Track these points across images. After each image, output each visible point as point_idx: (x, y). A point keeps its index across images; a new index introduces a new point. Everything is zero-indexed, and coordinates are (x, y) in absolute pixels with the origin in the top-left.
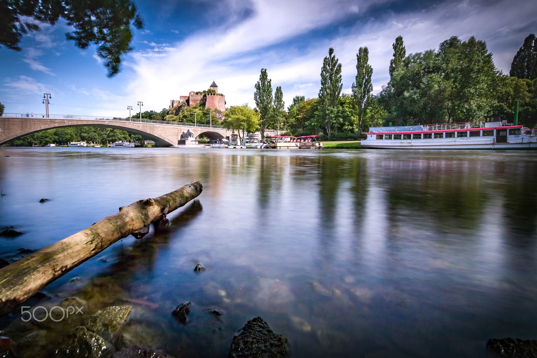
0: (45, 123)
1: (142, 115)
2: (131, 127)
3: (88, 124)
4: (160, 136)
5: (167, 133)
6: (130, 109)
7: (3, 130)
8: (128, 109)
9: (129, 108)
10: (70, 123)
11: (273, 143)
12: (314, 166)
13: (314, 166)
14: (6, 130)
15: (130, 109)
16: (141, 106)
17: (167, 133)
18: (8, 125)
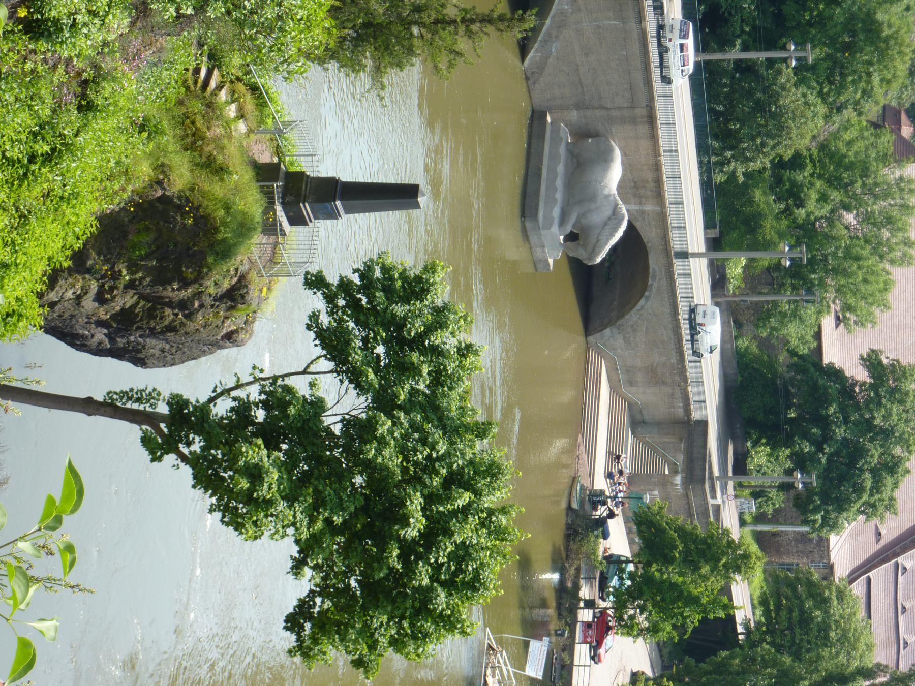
4: (561, 25)
17: (587, 55)
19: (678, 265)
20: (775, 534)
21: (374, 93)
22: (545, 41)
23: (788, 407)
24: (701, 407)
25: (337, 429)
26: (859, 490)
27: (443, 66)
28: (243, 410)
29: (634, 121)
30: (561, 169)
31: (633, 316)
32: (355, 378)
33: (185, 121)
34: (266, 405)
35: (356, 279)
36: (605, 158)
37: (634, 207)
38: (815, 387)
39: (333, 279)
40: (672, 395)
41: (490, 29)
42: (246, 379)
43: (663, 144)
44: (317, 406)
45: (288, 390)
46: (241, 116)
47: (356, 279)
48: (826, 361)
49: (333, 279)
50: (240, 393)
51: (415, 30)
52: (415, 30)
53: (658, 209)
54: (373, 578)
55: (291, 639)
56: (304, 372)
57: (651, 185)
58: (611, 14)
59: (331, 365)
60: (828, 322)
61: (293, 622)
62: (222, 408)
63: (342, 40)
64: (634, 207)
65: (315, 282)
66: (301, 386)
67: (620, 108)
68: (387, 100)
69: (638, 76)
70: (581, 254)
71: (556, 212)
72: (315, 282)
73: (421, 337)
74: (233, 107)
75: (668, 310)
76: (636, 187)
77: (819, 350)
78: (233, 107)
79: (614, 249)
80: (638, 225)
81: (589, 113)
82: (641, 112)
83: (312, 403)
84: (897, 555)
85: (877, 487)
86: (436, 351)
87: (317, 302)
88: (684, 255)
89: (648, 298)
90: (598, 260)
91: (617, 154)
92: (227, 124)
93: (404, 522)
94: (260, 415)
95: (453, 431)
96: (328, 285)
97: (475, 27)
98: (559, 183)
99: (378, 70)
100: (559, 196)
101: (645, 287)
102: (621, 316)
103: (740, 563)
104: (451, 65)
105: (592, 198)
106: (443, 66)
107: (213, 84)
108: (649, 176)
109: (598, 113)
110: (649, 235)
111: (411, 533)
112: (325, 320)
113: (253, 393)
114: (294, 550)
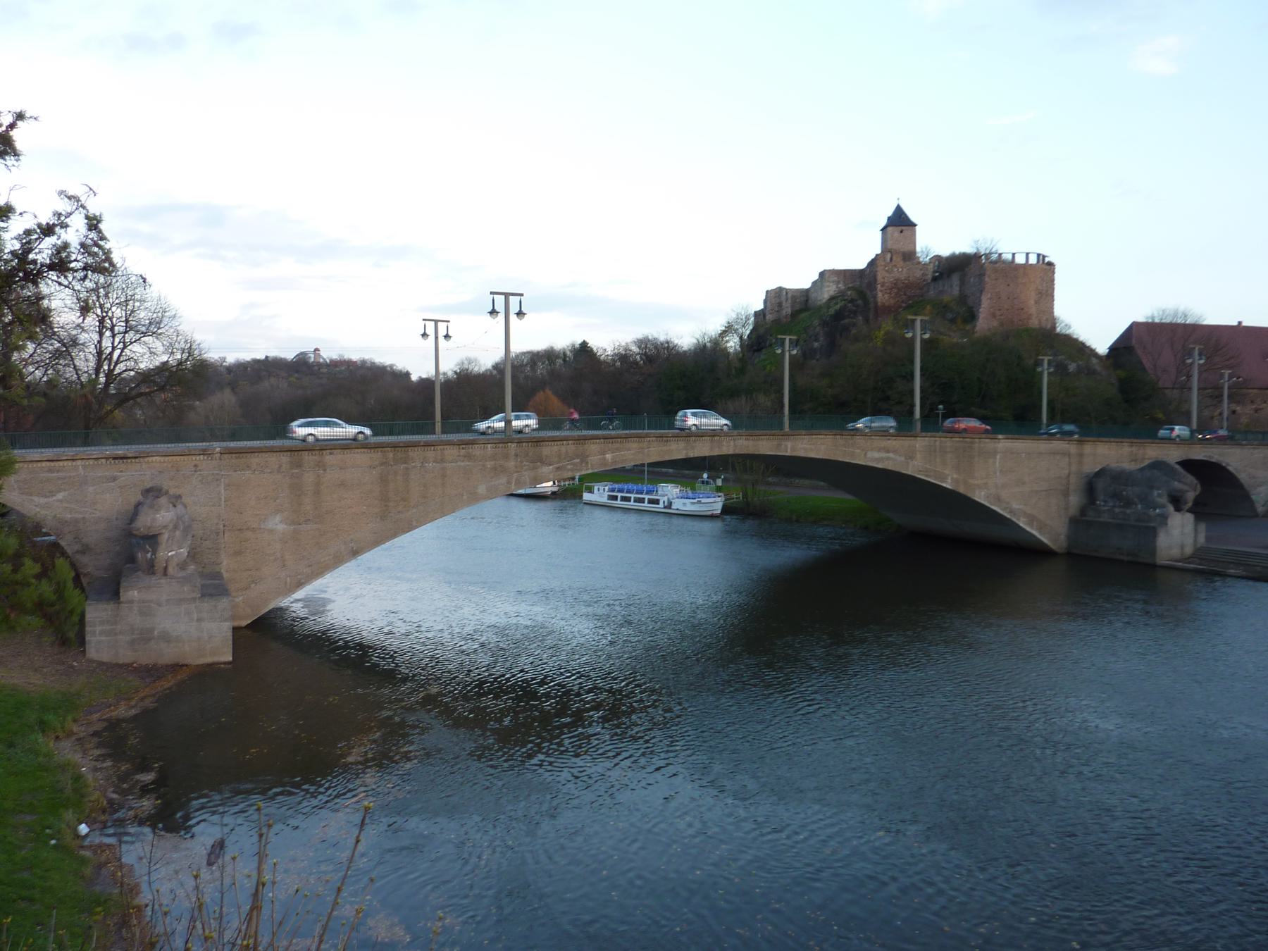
0: (495, 469)
1: (1199, 417)
2: (879, 460)
3: (691, 455)
4: (998, 499)
5: (1024, 483)
6: (436, 338)
7: (293, 523)
8: (424, 335)
9: (430, 331)
10: (609, 456)
11: (727, 525)
12: (575, 739)
13: (575, 739)
14: (307, 521)
15: (436, 338)
16: (513, 318)
17: (1024, 483)
18: (317, 493)
22: (1011, 512)
29: (1081, 455)
31: (1242, 477)
58: (991, 461)
67: (1070, 464)
81: (1072, 487)
89: (1228, 464)
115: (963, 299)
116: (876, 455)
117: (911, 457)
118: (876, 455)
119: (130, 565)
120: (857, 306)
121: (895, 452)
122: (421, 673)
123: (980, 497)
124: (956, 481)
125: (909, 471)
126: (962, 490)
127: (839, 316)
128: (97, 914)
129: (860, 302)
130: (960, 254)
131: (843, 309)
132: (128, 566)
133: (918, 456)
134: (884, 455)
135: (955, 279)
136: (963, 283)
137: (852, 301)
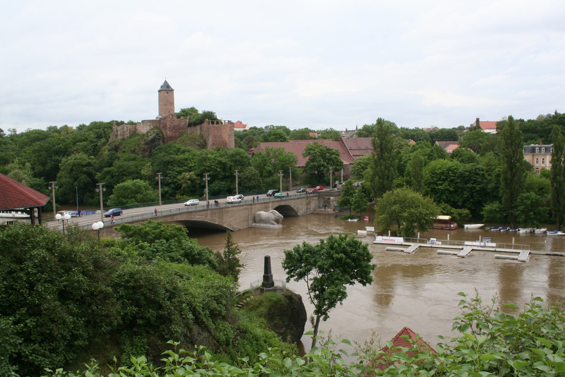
2: (199, 218)
4: (230, 225)
19: (158, 214)
20: (343, 177)
21: (245, 267)
23: (315, 173)
24: (99, 218)
25: (321, 275)
26: (336, 158)
27: (238, 251)
28: (316, 297)
29: (251, 209)
30: (262, 225)
31: (295, 208)
32: (309, 270)
33: (251, 310)
34: (315, 291)
35: (287, 270)
36: (259, 215)
37: (271, 208)
38: (311, 168)
39: (287, 276)
40: (313, 200)
41: (230, 241)
42: (309, 296)
43: (177, 212)
44: (315, 279)
45: (312, 285)
46: (249, 297)
47: (287, 270)
48: (304, 166)
49: (287, 276)
50: (312, 297)
51: (231, 257)
52: (231, 257)
53: (271, 203)
54: (436, 218)
55: (368, 285)
56: (307, 282)
57: (265, 204)
59: (306, 276)
60: (297, 165)
61: (364, 284)
62: (316, 301)
63: (232, 274)
64: (271, 208)
65: (288, 280)
66: (311, 282)
68: (246, 264)
69: (241, 208)
70: (281, 220)
71: (272, 226)
72: (288, 280)
73: (300, 255)
74: (247, 299)
75: (293, 201)
76: (266, 208)
77: (302, 167)
78: (247, 299)
79: (280, 213)
80: (274, 207)
81: (250, 219)
82: (249, 207)
83: (315, 280)
84: (347, 150)
85: (333, 154)
86: (304, 251)
87: (292, 279)
88: (156, 212)
90: (282, 216)
91: (259, 212)
92: (252, 300)
93: (341, 258)
94: (317, 292)
95: (322, 248)
96: (289, 277)
97: (230, 244)
98: (265, 225)
99: (240, 266)
100: (268, 225)
101: (288, 206)
102: (295, 211)
103: (350, 183)
104: (238, 249)
105: (269, 218)
106: (238, 251)
107: (242, 304)
108: (263, 205)
109: (250, 217)
110: (277, 205)
111: (344, 256)
112: (295, 278)
113: (312, 294)
114: (348, 285)
115: (202, 137)
116: (198, 217)
117: (207, 216)
118: (198, 217)
119: (196, 201)
120: (160, 136)
121: (203, 215)
122: (39, 351)
123: (225, 225)
124: (219, 222)
125: (206, 220)
126: (220, 224)
127: (153, 141)
128: (520, 199)
129: (160, 135)
130: (529, 121)
131: (154, 138)
132: (306, 340)
133: (209, 215)
134: (200, 217)
135: (198, 127)
136: (201, 129)
137: (157, 134)
